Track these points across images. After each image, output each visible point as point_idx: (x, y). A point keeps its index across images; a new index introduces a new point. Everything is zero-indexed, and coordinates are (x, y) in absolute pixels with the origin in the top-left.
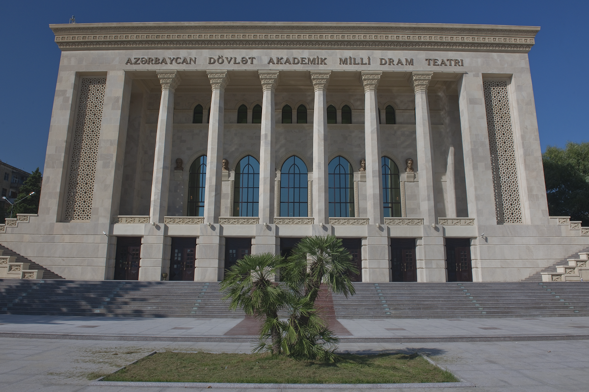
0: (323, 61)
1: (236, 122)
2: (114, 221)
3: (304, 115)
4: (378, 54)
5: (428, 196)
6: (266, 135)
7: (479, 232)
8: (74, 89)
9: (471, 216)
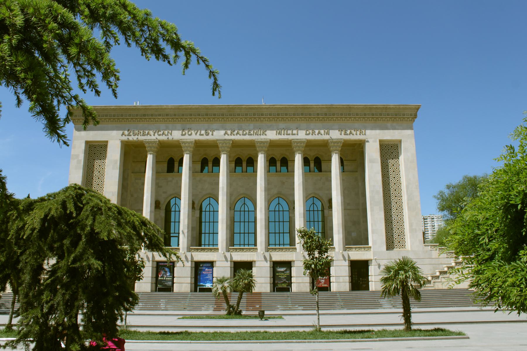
1: (200, 171)
3: (286, 163)
6: (223, 187)
7: (374, 257)
8: (85, 153)
9: (370, 244)
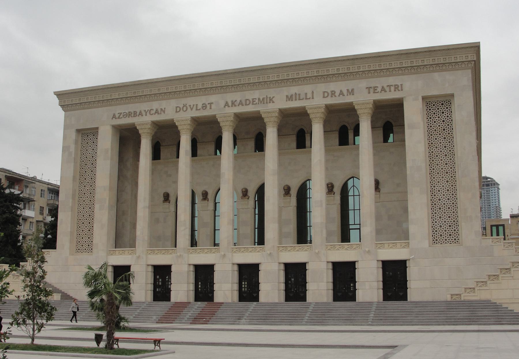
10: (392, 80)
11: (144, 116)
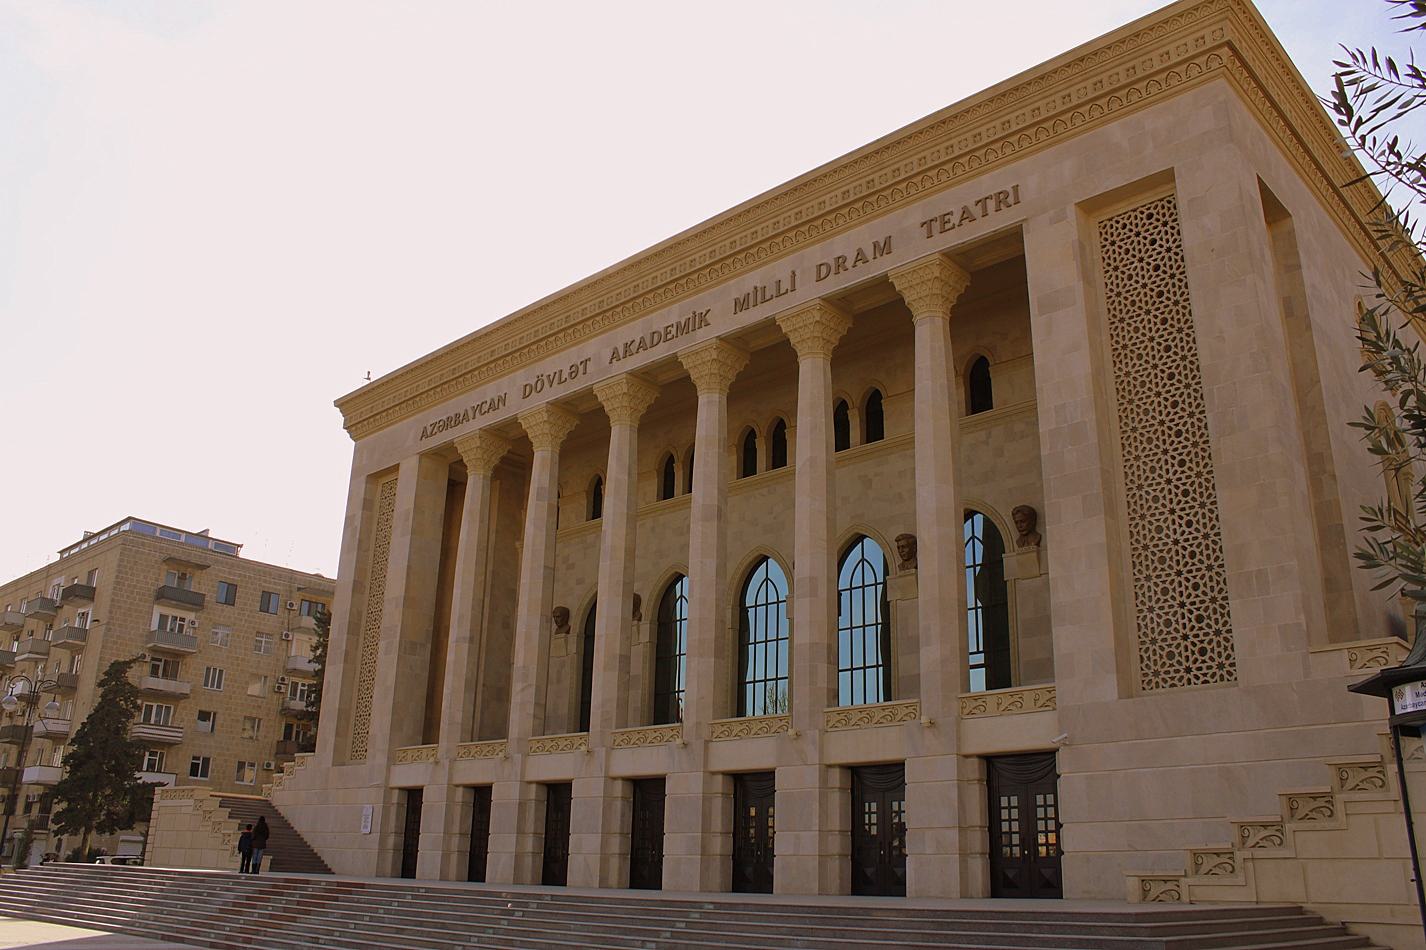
0: (701, 320)
2: (392, 760)
4: (913, 215)
5: (704, 799)
10: (988, 183)
11: (471, 420)
